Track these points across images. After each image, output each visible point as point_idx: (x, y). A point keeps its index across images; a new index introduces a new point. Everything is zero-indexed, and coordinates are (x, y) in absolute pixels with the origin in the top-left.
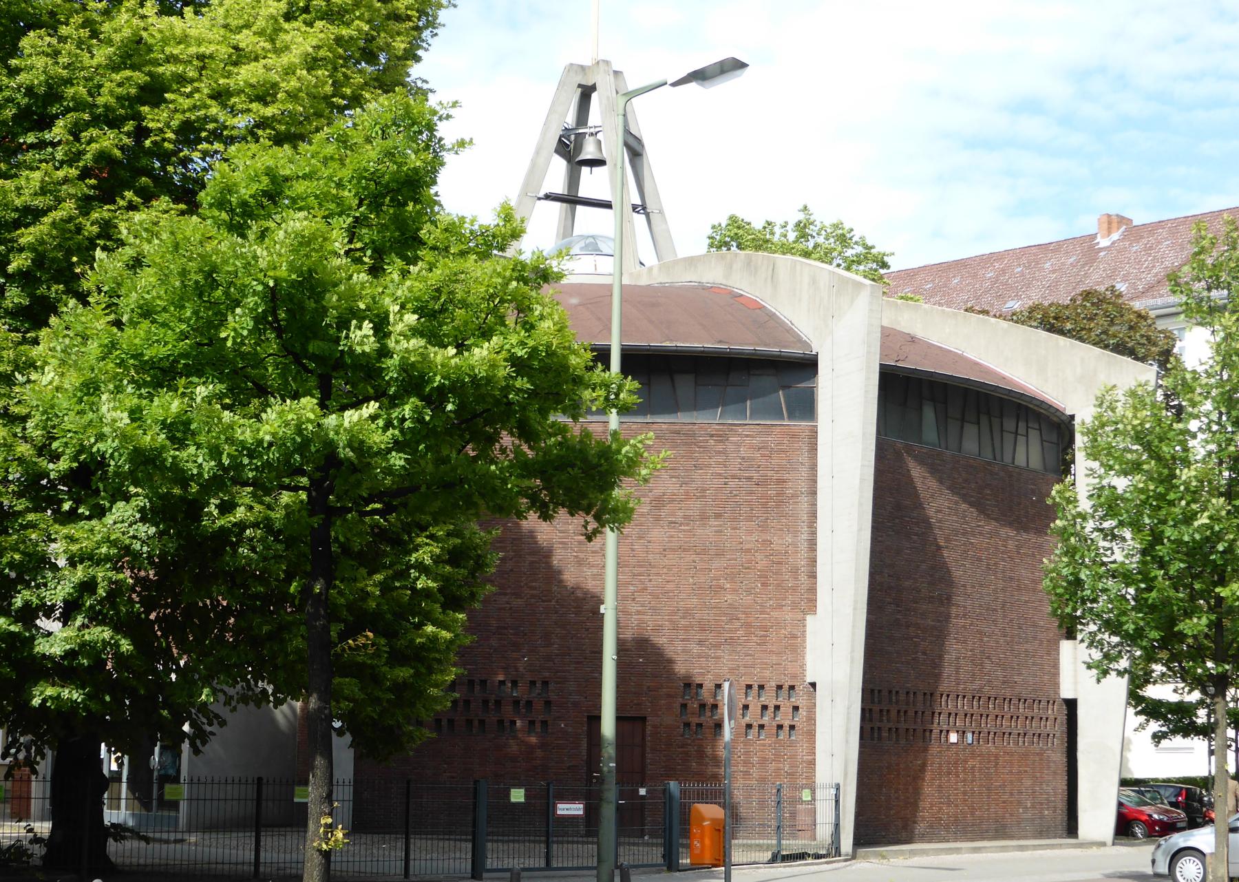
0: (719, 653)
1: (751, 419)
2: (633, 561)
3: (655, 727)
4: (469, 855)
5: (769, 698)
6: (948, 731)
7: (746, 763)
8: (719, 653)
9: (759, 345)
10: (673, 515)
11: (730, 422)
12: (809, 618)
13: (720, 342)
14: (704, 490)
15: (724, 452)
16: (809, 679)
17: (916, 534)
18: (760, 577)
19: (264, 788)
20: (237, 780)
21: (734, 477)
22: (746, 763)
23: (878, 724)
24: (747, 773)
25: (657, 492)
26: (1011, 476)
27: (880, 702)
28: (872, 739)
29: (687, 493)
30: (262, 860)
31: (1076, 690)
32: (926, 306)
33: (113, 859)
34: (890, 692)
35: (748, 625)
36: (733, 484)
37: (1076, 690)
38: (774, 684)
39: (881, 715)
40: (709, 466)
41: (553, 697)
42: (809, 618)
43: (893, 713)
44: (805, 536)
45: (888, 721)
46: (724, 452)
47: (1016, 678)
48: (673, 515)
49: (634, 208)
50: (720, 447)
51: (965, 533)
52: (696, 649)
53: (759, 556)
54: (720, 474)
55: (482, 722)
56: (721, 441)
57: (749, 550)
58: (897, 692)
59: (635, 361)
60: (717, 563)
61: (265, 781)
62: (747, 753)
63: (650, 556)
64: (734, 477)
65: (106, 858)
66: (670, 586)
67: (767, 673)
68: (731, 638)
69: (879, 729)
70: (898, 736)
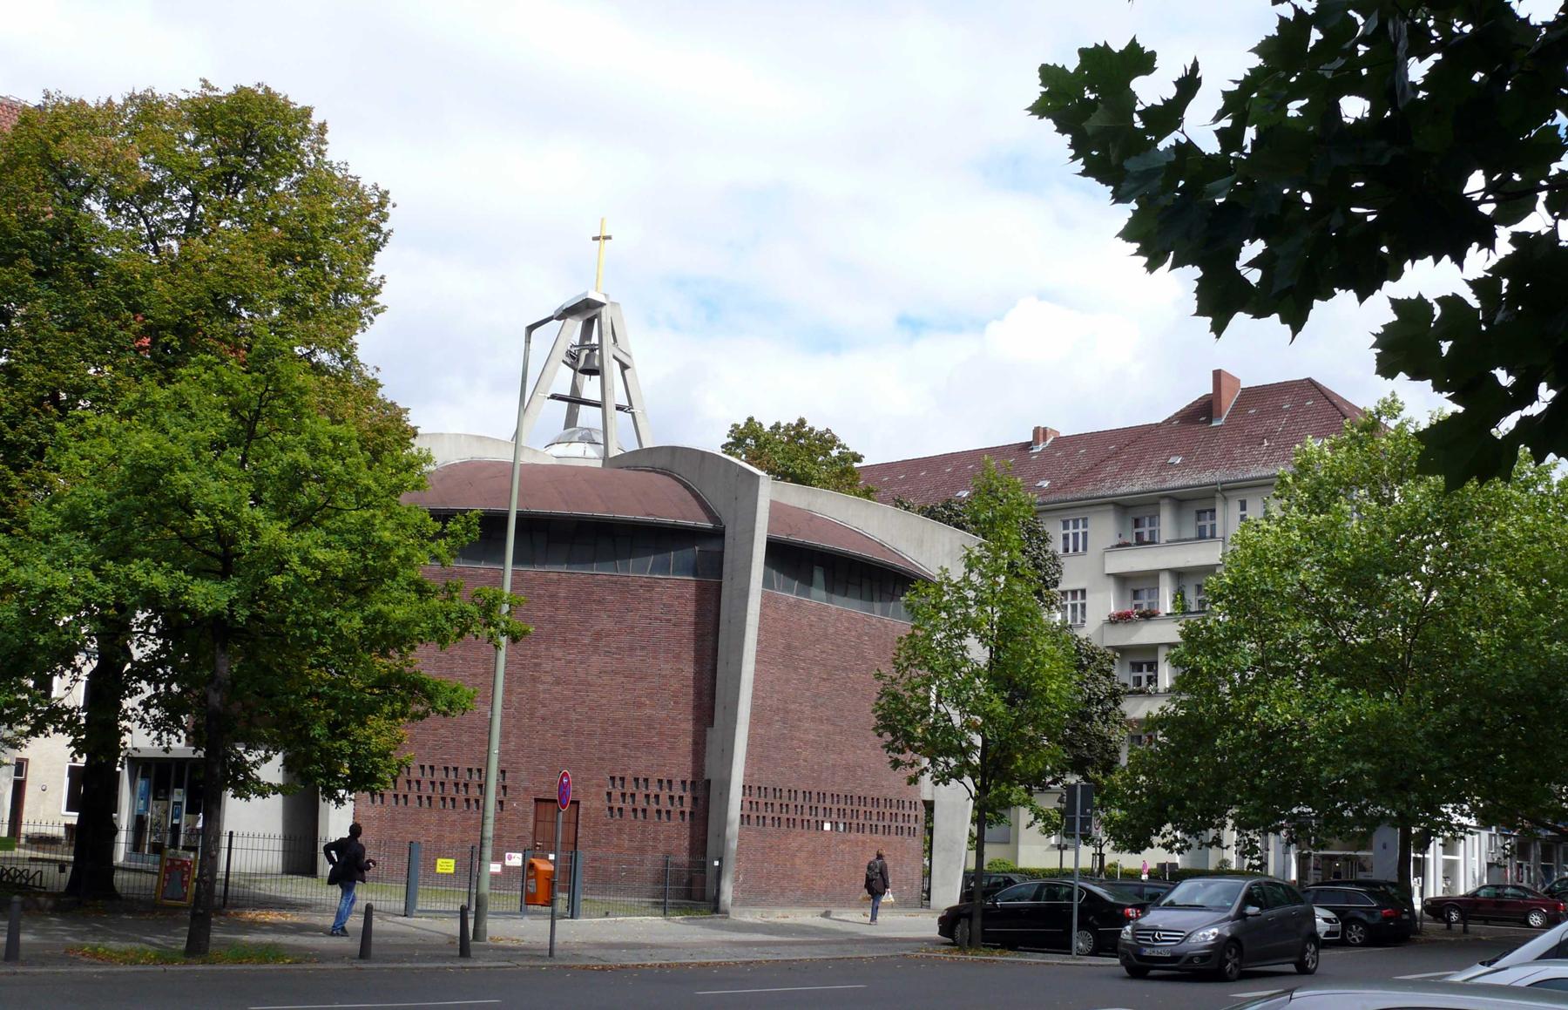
0: (639, 754)
1: (674, 574)
2: (576, 680)
3: (586, 809)
4: (404, 899)
5: (630, 788)
6: (823, 822)
7: (655, 839)
8: (639, 754)
9: (679, 518)
10: (609, 646)
11: (657, 576)
12: (708, 729)
13: (648, 515)
14: (633, 628)
15: (650, 599)
16: (706, 778)
17: (803, 669)
18: (673, 696)
19: (234, 839)
20: (262, 836)
21: (656, 619)
22: (655, 839)
23: (764, 814)
24: (655, 847)
25: (597, 628)
26: (886, 627)
27: (838, 802)
28: (758, 824)
29: (620, 630)
30: (229, 894)
31: (933, 794)
32: (1275, 514)
33: (118, 890)
34: (775, 789)
35: (660, 734)
36: (657, 624)
37: (933, 794)
38: (679, 779)
39: (782, 808)
40: (638, 610)
41: (508, 782)
42: (708, 729)
43: (777, 807)
44: (709, 667)
45: (772, 811)
46: (650, 599)
47: (884, 783)
48: (609, 646)
49: (619, 408)
50: (648, 595)
51: (845, 669)
52: (621, 751)
53: (672, 681)
54: (647, 617)
55: (405, 797)
56: (648, 591)
57: (665, 676)
58: (781, 790)
59: (528, 523)
60: (640, 685)
61: (234, 834)
62: (656, 832)
63: (589, 678)
64: (656, 619)
65: (112, 888)
66: (604, 701)
67: (674, 771)
68: (649, 743)
69: (764, 817)
70: (779, 824)
